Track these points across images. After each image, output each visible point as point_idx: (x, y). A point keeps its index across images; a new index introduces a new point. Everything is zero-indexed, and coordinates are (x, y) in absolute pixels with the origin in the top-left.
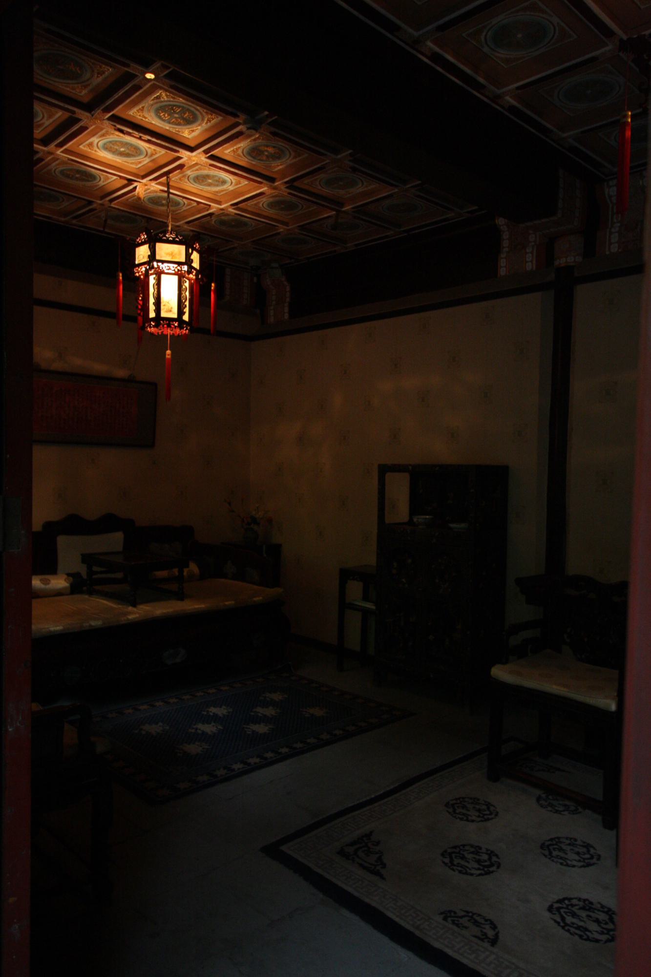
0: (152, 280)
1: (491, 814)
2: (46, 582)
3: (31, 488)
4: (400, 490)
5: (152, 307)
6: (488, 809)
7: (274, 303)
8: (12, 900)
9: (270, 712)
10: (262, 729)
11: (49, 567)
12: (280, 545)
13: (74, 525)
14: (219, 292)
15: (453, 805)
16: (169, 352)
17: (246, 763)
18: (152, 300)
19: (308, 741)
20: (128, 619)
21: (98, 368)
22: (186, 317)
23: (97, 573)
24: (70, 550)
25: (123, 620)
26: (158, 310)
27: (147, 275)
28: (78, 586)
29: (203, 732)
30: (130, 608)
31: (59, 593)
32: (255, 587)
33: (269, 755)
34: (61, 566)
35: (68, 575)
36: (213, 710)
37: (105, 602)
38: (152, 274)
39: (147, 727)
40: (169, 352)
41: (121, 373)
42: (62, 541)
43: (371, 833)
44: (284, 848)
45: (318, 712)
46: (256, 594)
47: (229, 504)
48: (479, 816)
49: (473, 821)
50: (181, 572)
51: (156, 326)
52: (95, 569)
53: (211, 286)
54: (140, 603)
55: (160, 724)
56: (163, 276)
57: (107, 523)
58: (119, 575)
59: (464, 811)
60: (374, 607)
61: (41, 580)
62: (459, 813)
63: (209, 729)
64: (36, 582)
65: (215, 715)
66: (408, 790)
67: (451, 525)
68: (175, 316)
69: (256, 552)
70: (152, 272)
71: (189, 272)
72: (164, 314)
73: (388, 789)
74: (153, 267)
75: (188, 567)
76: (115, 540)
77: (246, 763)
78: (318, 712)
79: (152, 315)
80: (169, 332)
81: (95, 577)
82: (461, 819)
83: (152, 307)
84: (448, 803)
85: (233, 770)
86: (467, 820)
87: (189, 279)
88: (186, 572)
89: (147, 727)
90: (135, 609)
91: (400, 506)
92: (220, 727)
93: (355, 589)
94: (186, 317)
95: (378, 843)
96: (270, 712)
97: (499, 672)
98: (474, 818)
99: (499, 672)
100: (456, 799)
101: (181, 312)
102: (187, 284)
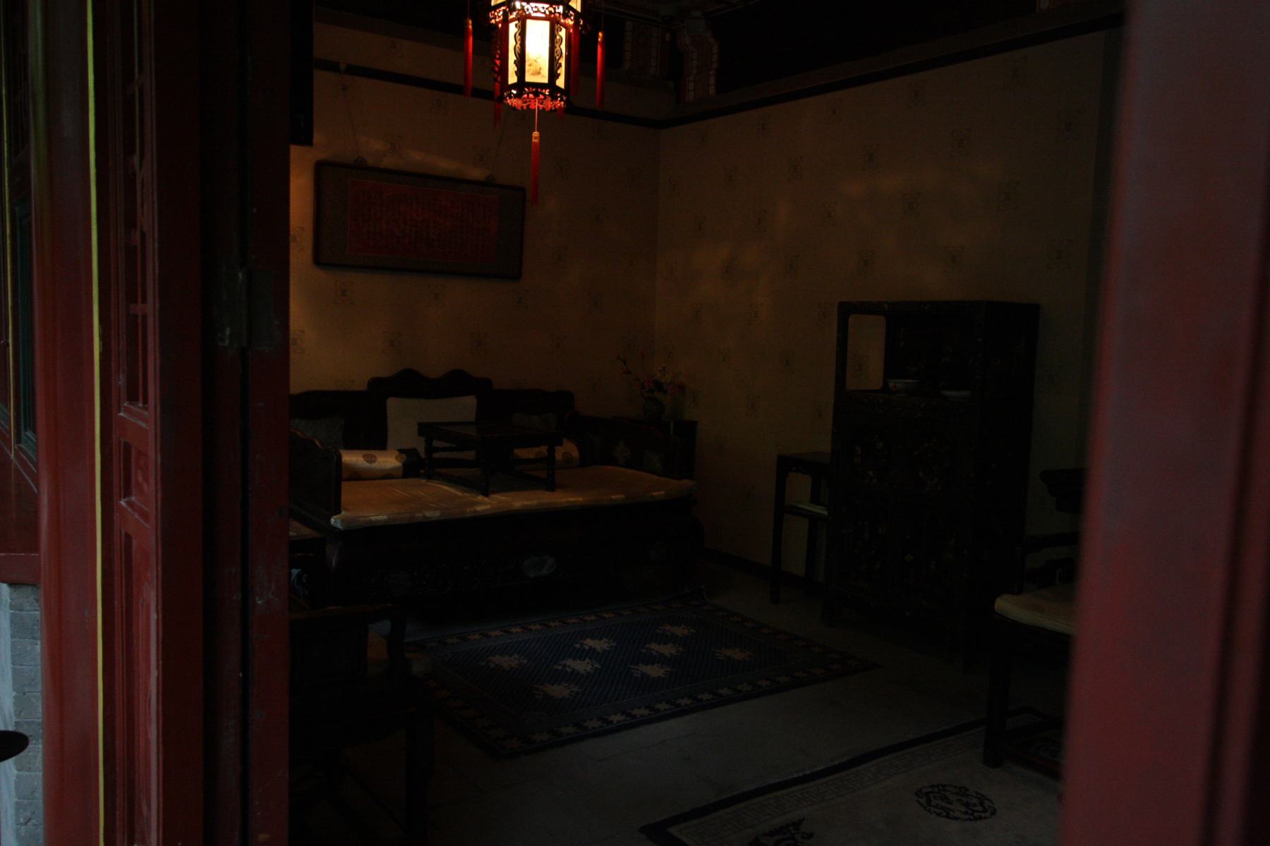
0: (513, 29)
1: (985, 811)
2: (371, 459)
3: (288, 253)
4: (870, 341)
5: (512, 68)
6: (982, 804)
7: (695, 71)
8: (263, 837)
9: (668, 650)
10: (655, 671)
11: (376, 440)
12: (696, 423)
13: (409, 383)
14: (613, 59)
15: (927, 794)
16: (536, 134)
17: (629, 715)
18: (512, 58)
19: (721, 691)
20: (475, 511)
21: (446, 165)
22: (561, 82)
23: (438, 450)
24: (403, 417)
25: (469, 512)
26: (521, 72)
27: (506, 22)
28: (413, 467)
29: (573, 670)
30: (480, 498)
31: (387, 475)
32: (655, 477)
33: (662, 706)
34: (389, 442)
35: (401, 451)
36: (590, 643)
37: (446, 488)
38: (513, 20)
39: (497, 659)
40: (536, 134)
41: (477, 173)
42: (393, 404)
43: (801, 821)
44: (673, 830)
45: (736, 654)
46: (656, 487)
47: (625, 362)
48: (966, 813)
49: (956, 818)
50: (551, 451)
51: (518, 96)
52: (436, 444)
53: (597, 36)
54: (494, 492)
55: (516, 656)
56: (529, 22)
57: (455, 383)
58: (470, 455)
59: (944, 804)
60: (826, 513)
61: (364, 456)
62: (937, 806)
63: (582, 666)
64: (353, 458)
65: (592, 649)
66: (860, 768)
67: (946, 393)
68: (546, 80)
69: (661, 430)
70: (514, 15)
71: (566, 16)
72: (529, 78)
73: (831, 764)
74: (514, 9)
75: (561, 444)
76: (464, 408)
77: (629, 715)
78: (736, 654)
79: (513, 79)
80: (536, 105)
81: (435, 455)
82: (938, 815)
83: (512, 68)
84: (920, 790)
85: (611, 722)
86: (948, 817)
87: (566, 27)
88: (559, 453)
89: (497, 659)
90: (486, 499)
91: (870, 370)
92: (598, 666)
93: (800, 487)
94: (561, 82)
95: (810, 836)
96: (668, 650)
97: (1006, 605)
98: (958, 814)
99: (1006, 605)
100: (932, 786)
101: (553, 75)
102: (563, 33)
